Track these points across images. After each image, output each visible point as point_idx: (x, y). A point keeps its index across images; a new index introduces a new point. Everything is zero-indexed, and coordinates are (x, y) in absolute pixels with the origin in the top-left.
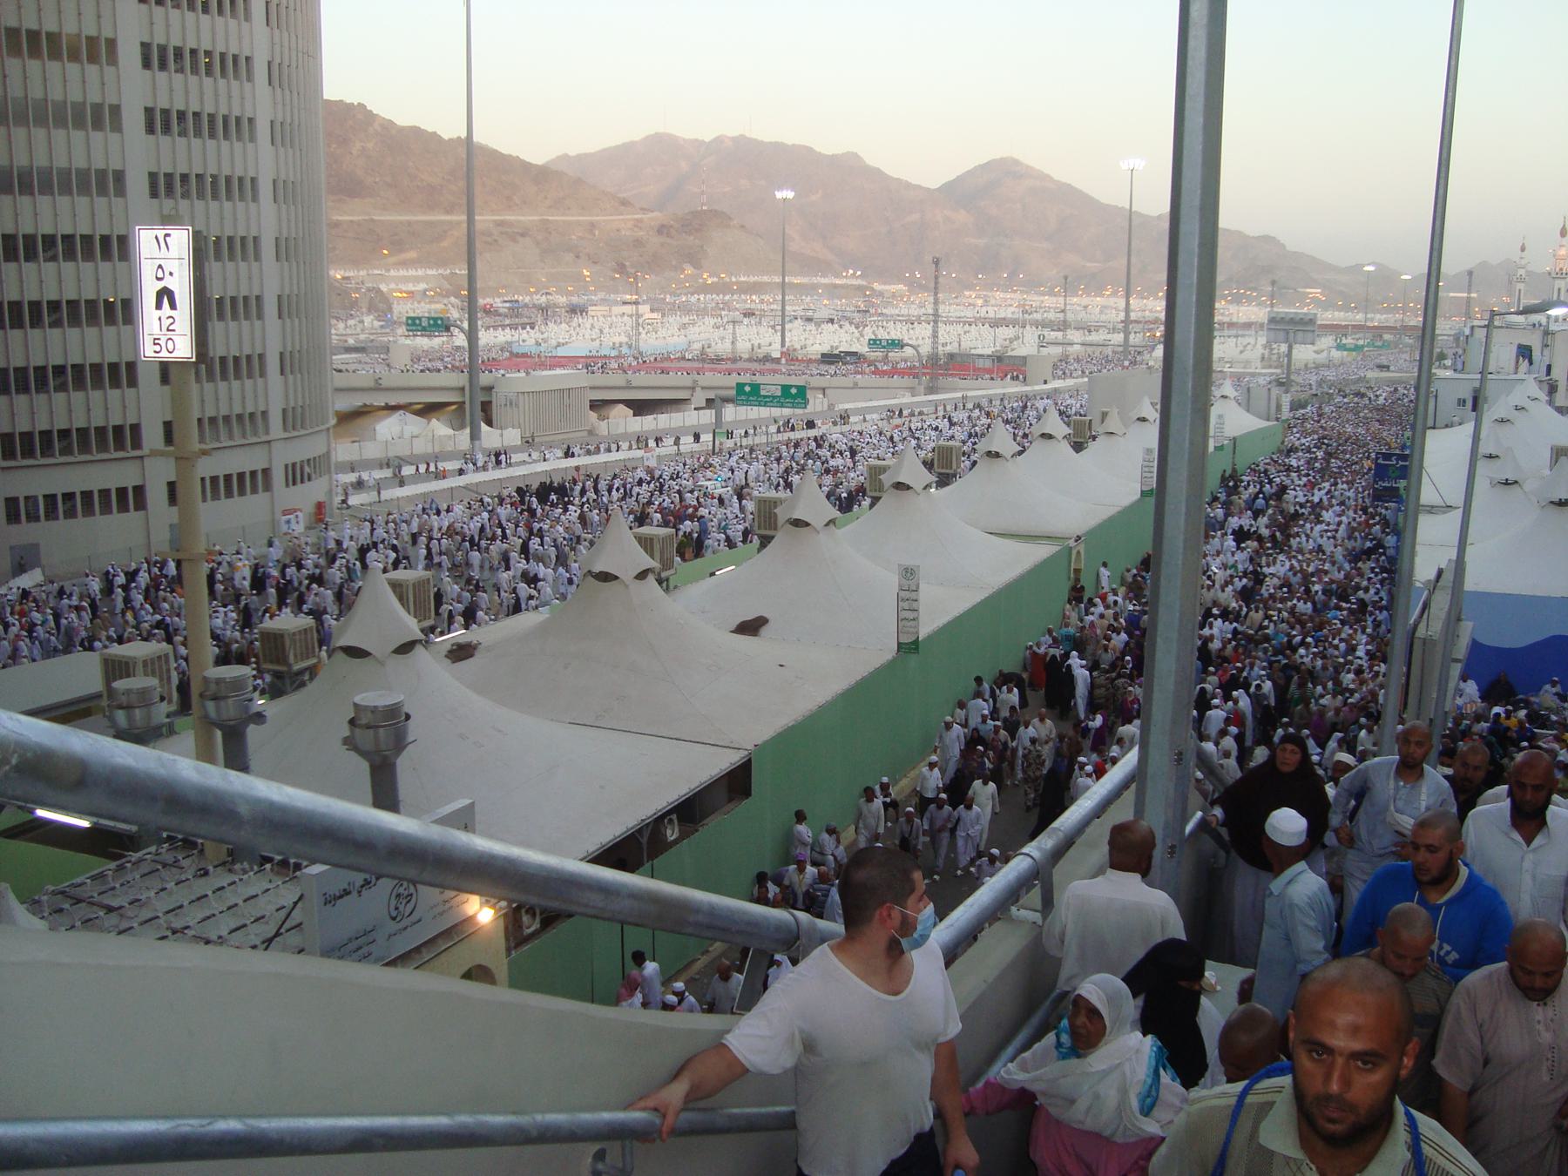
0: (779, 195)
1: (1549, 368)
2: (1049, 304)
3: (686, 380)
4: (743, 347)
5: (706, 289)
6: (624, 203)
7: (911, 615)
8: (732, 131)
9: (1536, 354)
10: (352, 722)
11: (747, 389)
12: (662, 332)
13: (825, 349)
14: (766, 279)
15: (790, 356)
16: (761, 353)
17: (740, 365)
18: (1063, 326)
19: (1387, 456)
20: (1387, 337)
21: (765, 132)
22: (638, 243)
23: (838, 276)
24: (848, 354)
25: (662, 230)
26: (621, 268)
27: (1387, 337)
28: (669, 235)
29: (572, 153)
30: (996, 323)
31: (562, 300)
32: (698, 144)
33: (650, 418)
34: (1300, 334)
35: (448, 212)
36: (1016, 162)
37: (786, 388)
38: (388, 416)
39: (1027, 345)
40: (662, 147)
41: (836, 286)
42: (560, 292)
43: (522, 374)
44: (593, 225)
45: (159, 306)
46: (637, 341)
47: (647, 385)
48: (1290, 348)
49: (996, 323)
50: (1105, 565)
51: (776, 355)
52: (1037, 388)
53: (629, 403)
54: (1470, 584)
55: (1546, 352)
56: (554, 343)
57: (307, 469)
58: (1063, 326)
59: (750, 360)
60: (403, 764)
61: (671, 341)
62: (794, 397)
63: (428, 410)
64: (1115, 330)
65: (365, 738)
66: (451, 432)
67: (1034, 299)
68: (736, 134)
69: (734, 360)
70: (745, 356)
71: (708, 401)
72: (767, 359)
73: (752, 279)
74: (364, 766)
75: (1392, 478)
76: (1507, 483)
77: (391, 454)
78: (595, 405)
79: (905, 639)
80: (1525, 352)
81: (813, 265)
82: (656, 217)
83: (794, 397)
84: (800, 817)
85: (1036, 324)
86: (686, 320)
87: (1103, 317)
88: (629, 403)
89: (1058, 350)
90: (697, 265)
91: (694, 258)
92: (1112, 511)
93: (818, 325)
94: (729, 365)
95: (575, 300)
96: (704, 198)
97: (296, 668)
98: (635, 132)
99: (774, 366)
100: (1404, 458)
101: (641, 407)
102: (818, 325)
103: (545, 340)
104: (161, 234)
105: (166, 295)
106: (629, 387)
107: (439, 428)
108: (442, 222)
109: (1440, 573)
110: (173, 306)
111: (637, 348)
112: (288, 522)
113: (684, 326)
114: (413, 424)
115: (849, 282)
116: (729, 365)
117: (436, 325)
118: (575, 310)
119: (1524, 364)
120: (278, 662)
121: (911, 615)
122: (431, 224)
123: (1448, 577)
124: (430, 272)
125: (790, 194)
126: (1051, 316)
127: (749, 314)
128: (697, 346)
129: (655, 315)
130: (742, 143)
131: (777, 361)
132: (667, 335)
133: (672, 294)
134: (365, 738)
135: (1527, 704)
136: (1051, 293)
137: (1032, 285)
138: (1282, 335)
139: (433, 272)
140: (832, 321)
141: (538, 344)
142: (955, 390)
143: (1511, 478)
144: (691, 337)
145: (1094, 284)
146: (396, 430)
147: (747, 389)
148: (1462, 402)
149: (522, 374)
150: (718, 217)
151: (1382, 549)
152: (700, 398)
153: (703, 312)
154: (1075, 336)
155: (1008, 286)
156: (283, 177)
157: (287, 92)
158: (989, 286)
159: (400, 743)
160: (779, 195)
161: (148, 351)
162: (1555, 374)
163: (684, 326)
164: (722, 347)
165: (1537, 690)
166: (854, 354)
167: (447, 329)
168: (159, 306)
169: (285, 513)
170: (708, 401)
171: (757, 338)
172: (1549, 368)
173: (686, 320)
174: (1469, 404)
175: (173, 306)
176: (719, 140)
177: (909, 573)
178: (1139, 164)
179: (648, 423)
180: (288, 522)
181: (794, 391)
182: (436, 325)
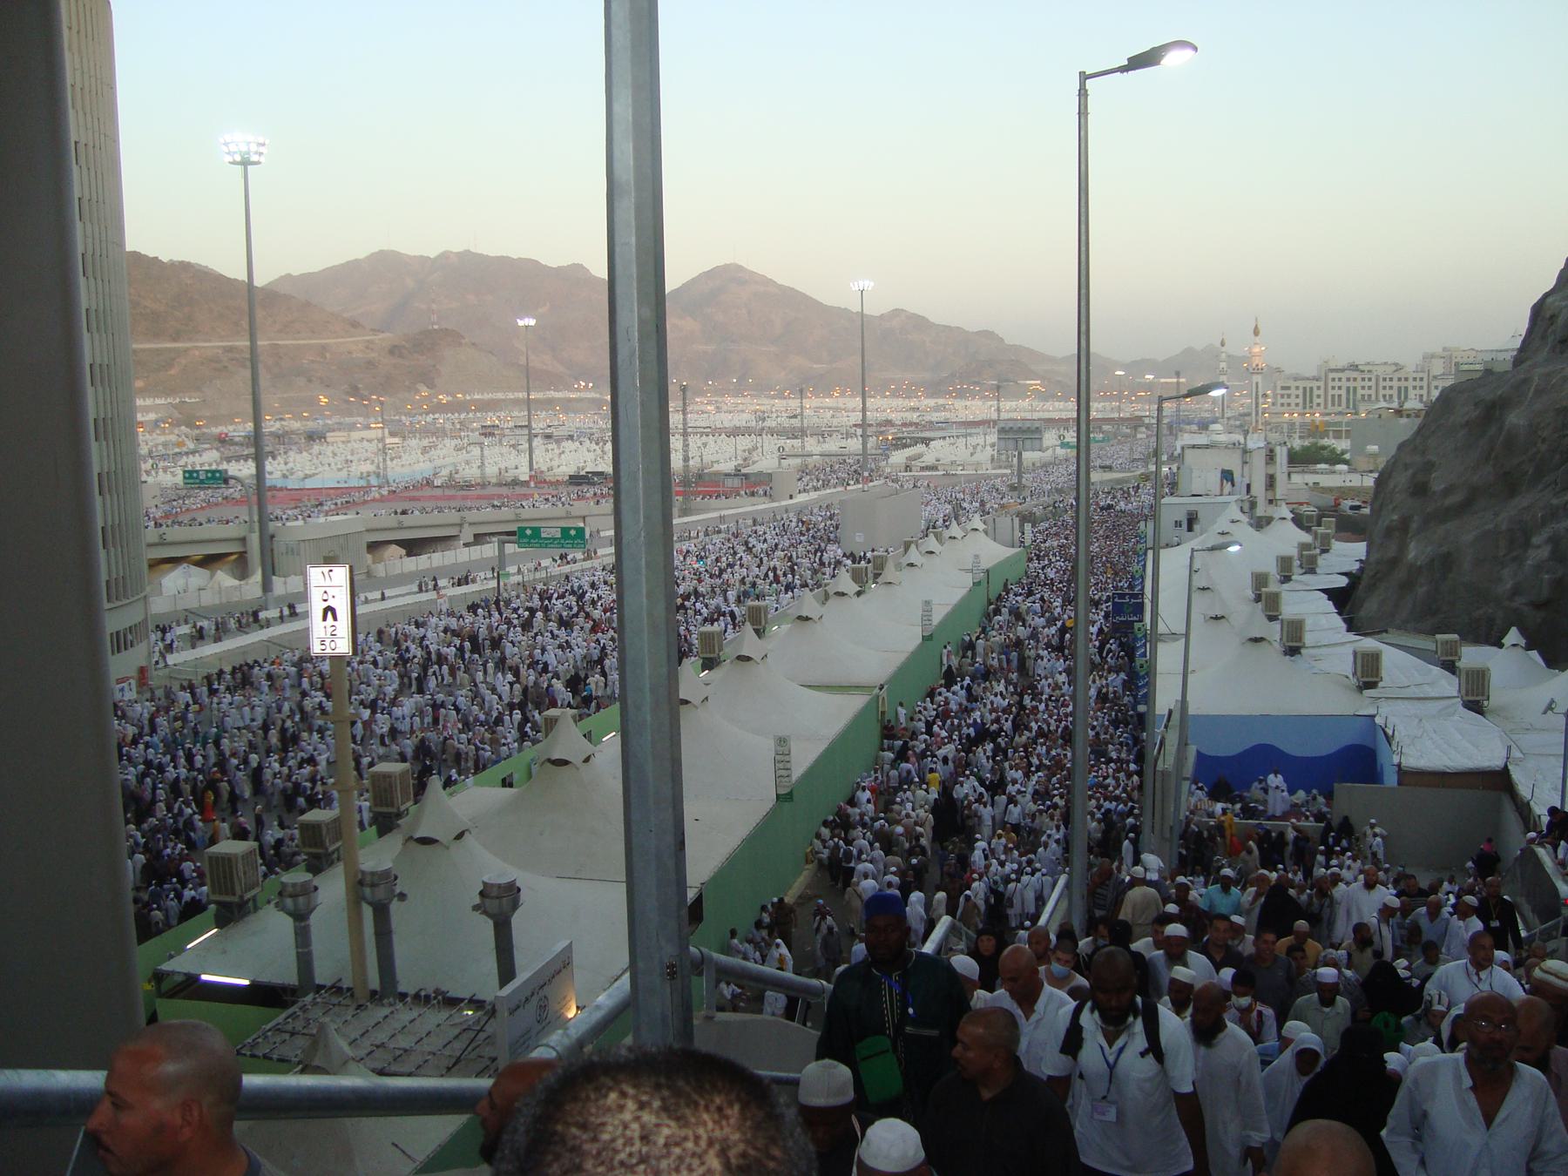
0: (521, 323)
1: (1249, 486)
2: (780, 409)
3: (452, 516)
4: (491, 471)
5: (441, 408)
6: (355, 324)
7: (784, 773)
8: (457, 248)
9: (1237, 476)
10: (481, 893)
11: (529, 532)
12: (406, 458)
13: (572, 470)
14: (500, 396)
15: (538, 479)
16: (509, 476)
17: (490, 491)
18: (799, 433)
19: (1122, 596)
20: (1105, 428)
21: (491, 247)
22: (370, 364)
23: (570, 389)
24: (594, 474)
25: (394, 350)
26: (354, 391)
27: (1105, 428)
28: (401, 356)
29: (295, 273)
30: (734, 432)
31: (296, 425)
32: (423, 260)
33: (424, 557)
34: (1028, 442)
35: (174, 340)
36: (740, 268)
37: (565, 531)
38: (172, 570)
39: (766, 462)
40: (385, 265)
41: (570, 400)
42: (298, 417)
43: (300, 523)
44: (324, 348)
45: (325, 619)
46: (385, 469)
47: (419, 522)
48: (1020, 454)
49: (734, 432)
50: (901, 704)
51: (525, 478)
52: (784, 503)
53: (400, 543)
54: (1192, 711)
55: (1246, 468)
56: (301, 475)
57: (130, 637)
58: (794, 433)
59: (500, 485)
60: (516, 920)
61: (417, 467)
62: (574, 538)
63: (208, 562)
64: (848, 435)
65: (492, 905)
66: (236, 582)
67: (764, 404)
68: (460, 249)
69: (483, 485)
70: (494, 481)
71: (476, 536)
72: (515, 482)
73: (487, 396)
74: (491, 922)
75: (1127, 634)
76: (1216, 618)
77: (179, 607)
78: (373, 547)
79: (782, 791)
80: (1227, 476)
81: (555, 381)
82: (385, 338)
83: (574, 538)
84: (733, 934)
85: (772, 432)
86: (425, 442)
87: (835, 422)
88: (400, 543)
89: (798, 461)
90: (431, 386)
91: (427, 378)
92: (902, 658)
93: (558, 442)
94: (479, 492)
95: (311, 425)
96: (434, 318)
97: (331, 849)
98: (357, 246)
99: (524, 490)
100: (1135, 596)
101: (413, 547)
102: (558, 442)
103: (292, 472)
104: (325, 570)
105: (329, 611)
106: (401, 528)
107: (224, 578)
108: (170, 350)
109: (1170, 712)
110: (335, 619)
111: (385, 476)
112: (122, 690)
113: (425, 450)
114: (197, 576)
115: (583, 395)
116: (479, 492)
117: (214, 477)
118: (313, 437)
119: (1228, 486)
120: (316, 846)
121: (784, 773)
122: (158, 352)
123: (1176, 717)
124: (158, 401)
125: (532, 322)
126: (787, 423)
127: (488, 431)
128: (445, 472)
129: (396, 440)
130: (467, 257)
131: (526, 484)
132: (412, 462)
133: (408, 414)
134: (492, 905)
135: (1242, 799)
136: (781, 396)
137: (762, 388)
138: (1011, 444)
139: (162, 401)
140: (571, 437)
141: (285, 476)
142: (707, 510)
143: (1219, 614)
144: (439, 462)
145: (822, 385)
146: (181, 582)
147: (529, 532)
148: (1178, 524)
149: (300, 523)
150: (453, 337)
151: (1130, 713)
152: (467, 534)
153: (440, 433)
154: (811, 445)
155: (738, 392)
156: (98, 361)
157: (92, 280)
158: (722, 392)
159: (515, 905)
160: (521, 323)
161: (316, 649)
162: (1254, 491)
163: (425, 450)
164: (470, 473)
165: (1248, 787)
166: (601, 474)
167: (226, 481)
168: (325, 619)
169: (119, 681)
170: (476, 536)
171: (503, 460)
172: (1249, 486)
173: (425, 442)
174: (1185, 526)
175: (335, 619)
176: (445, 255)
177: (782, 741)
178: (868, 284)
179: (423, 562)
180: (122, 690)
181: (573, 533)
182: (214, 477)
